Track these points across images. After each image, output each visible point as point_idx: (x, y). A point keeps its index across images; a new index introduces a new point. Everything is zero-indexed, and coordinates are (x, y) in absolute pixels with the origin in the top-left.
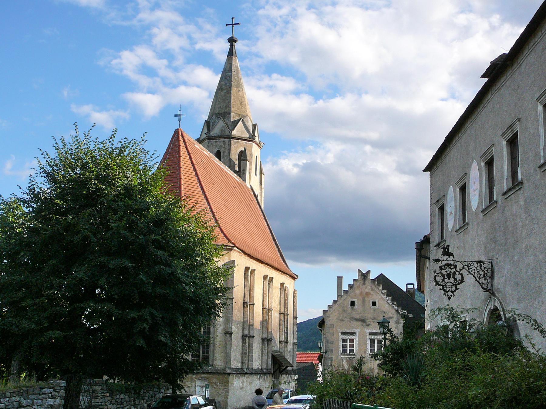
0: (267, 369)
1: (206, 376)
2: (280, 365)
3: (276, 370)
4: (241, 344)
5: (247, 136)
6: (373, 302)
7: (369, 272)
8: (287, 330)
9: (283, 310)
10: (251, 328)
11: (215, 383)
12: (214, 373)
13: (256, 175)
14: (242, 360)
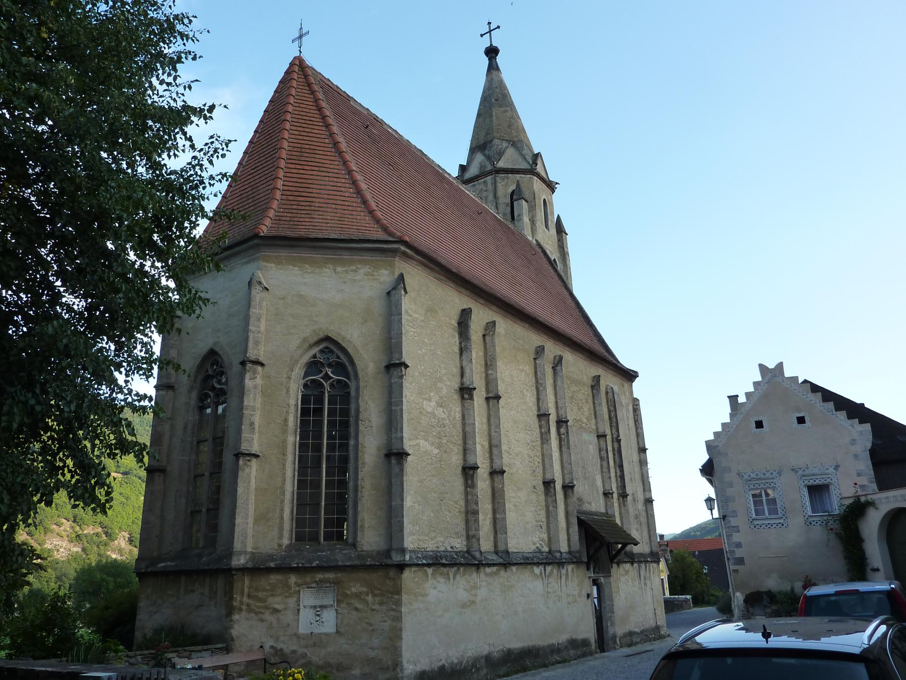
0: (570, 552)
1: (331, 576)
5: (524, 166)
6: (761, 422)
10: (495, 451)
11: (358, 596)
12: (354, 568)
13: (547, 226)
14: (468, 529)
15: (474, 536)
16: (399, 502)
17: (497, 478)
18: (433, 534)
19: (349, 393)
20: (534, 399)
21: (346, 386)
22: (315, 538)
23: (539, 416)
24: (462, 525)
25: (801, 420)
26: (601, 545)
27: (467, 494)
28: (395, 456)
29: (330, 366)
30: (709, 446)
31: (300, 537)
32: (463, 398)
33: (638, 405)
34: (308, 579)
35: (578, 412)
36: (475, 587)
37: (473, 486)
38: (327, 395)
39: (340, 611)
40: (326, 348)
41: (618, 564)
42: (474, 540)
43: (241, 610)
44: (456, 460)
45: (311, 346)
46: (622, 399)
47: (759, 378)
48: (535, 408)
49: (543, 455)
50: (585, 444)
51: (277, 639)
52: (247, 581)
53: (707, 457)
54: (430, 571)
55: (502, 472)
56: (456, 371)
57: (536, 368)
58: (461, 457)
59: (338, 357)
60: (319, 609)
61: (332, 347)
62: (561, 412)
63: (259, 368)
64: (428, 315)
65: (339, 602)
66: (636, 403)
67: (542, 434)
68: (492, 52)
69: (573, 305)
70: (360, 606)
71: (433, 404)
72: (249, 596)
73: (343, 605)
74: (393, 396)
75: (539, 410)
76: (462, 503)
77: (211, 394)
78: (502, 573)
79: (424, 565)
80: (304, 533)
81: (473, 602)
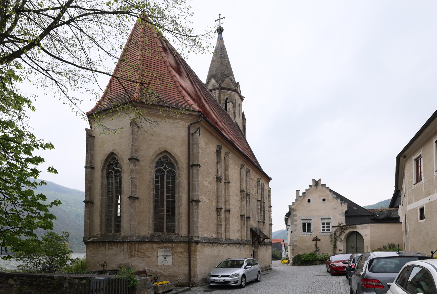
1: (170, 245)
2: (259, 237)
3: (256, 241)
4: (216, 216)
7: (320, 180)
8: (264, 214)
9: (260, 198)
10: (227, 203)
11: (181, 252)
14: (217, 230)
15: (220, 233)
16: (196, 219)
17: (227, 213)
18: (206, 232)
19: (175, 176)
20: (239, 184)
21: (174, 173)
22: (162, 231)
23: (241, 191)
24: (215, 229)
25: (324, 200)
26: (258, 238)
27: (218, 218)
28: (193, 202)
29: (167, 163)
30: (290, 207)
31: (156, 230)
32: (217, 181)
33: (270, 190)
34: (161, 246)
35: (253, 191)
36: (220, 251)
37: (220, 215)
38: (165, 176)
39: (174, 257)
40: (165, 156)
41: (260, 245)
42: (219, 234)
43: (135, 256)
44: (214, 205)
45: (159, 154)
46: (266, 188)
47: (311, 184)
48: (239, 188)
49: (241, 206)
50: (254, 204)
51: (150, 267)
52: (137, 246)
53: (289, 211)
54: (206, 245)
55: (229, 211)
56: (215, 170)
57: (241, 172)
58: (216, 204)
59: (170, 160)
60: (165, 257)
61: (168, 155)
62: (248, 190)
63: (137, 162)
64: (206, 147)
65: (173, 254)
66: (270, 189)
67: (241, 198)
68: (220, 31)
69: (433, 123)
70: (181, 256)
71: (207, 183)
72: (138, 251)
73: (175, 255)
74: (194, 178)
75: (241, 189)
76: (216, 221)
77: (113, 172)
78: (228, 246)
79: (204, 242)
80: (158, 229)
81: (219, 256)
